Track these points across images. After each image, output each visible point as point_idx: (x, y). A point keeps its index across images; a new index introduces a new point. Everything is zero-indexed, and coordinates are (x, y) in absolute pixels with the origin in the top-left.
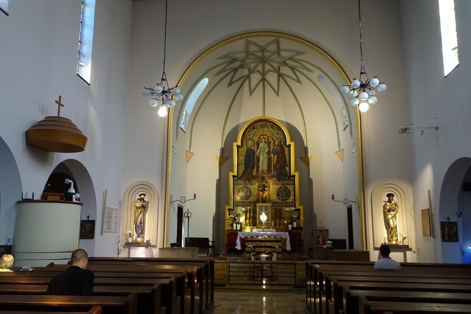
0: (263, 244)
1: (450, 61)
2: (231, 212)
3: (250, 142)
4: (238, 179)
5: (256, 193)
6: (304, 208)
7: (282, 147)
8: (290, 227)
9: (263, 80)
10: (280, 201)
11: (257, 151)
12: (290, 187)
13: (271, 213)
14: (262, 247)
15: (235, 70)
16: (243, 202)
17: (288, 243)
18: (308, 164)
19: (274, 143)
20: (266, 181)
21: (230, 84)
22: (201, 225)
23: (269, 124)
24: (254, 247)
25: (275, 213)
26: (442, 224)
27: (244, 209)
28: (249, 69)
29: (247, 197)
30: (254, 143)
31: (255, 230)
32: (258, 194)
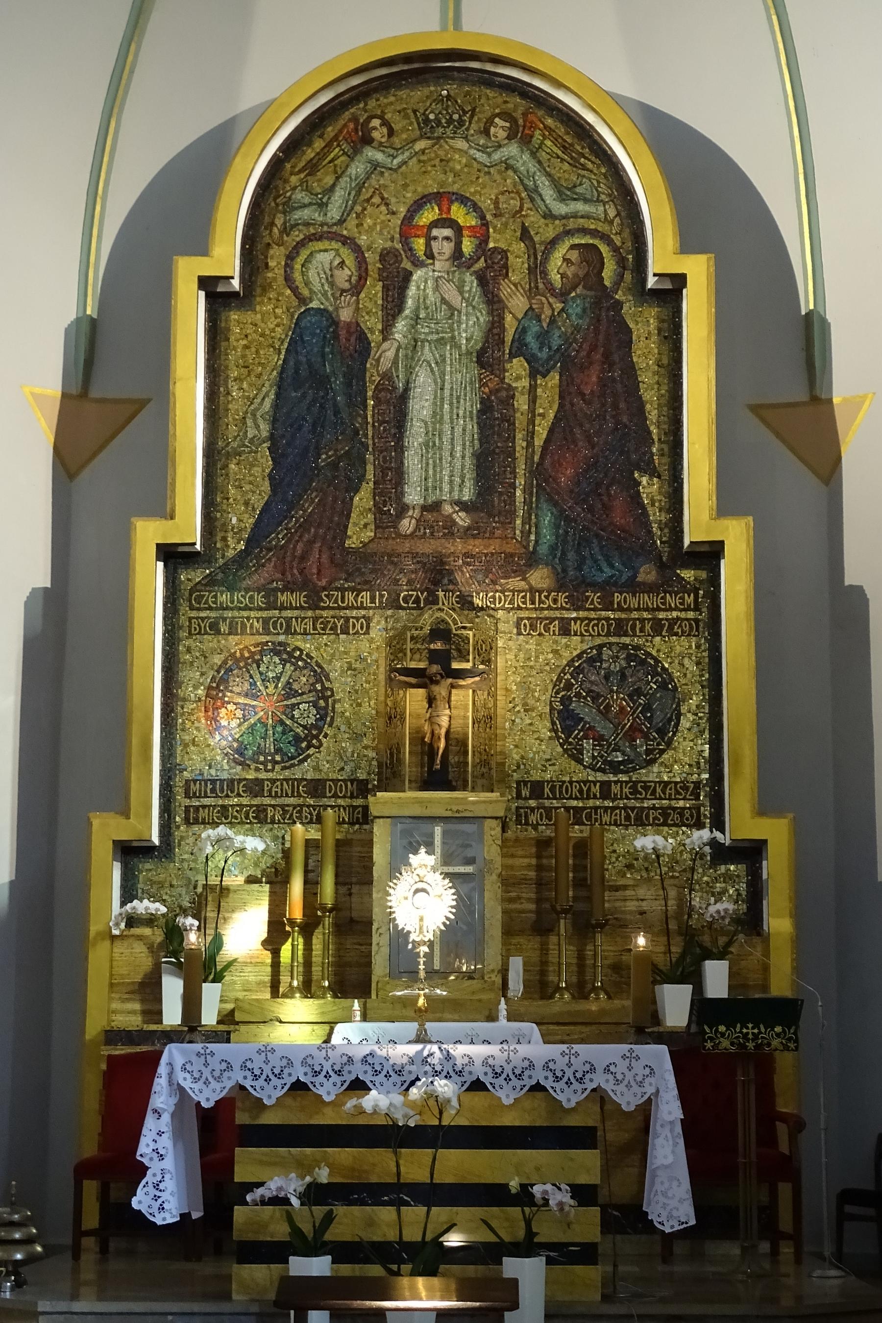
0: (415, 1165)
2: (147, 869)
3: (324, 259)
4: (210, 582)
5: (368, 709)
6: (799, 834)
7: (603, 305)
8: (675, 1005)
10: (582, 774)
11: (386, 332)
12: (679, 656)
13: (507, 882)
14: (397, 1193)
16: (255, 788)
17: (668, 1151)
18: (827, 467)
19: (537, 270)
20: (465, 603)
23: (490, 100)
24: (315, 1194)
25: (540, 884)
27: (254, 844)
30: (361, 262)
31: (353, 1034)
32: (393, 716)
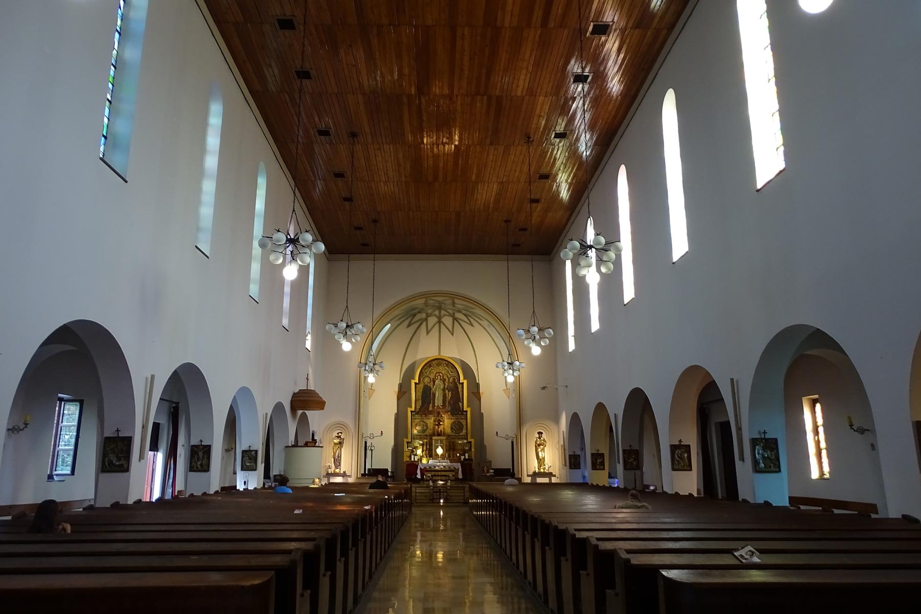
1: (572, 346)
8: (463, 457)
9: (440, 322)
12: (464, 422)
15: (414, 315)
17: (460, 472)
21: (409, 326)
22: (383, 459)
26: (592, 455)
28: (427, 314)
29: (424, 431)
31: (431, 462)
